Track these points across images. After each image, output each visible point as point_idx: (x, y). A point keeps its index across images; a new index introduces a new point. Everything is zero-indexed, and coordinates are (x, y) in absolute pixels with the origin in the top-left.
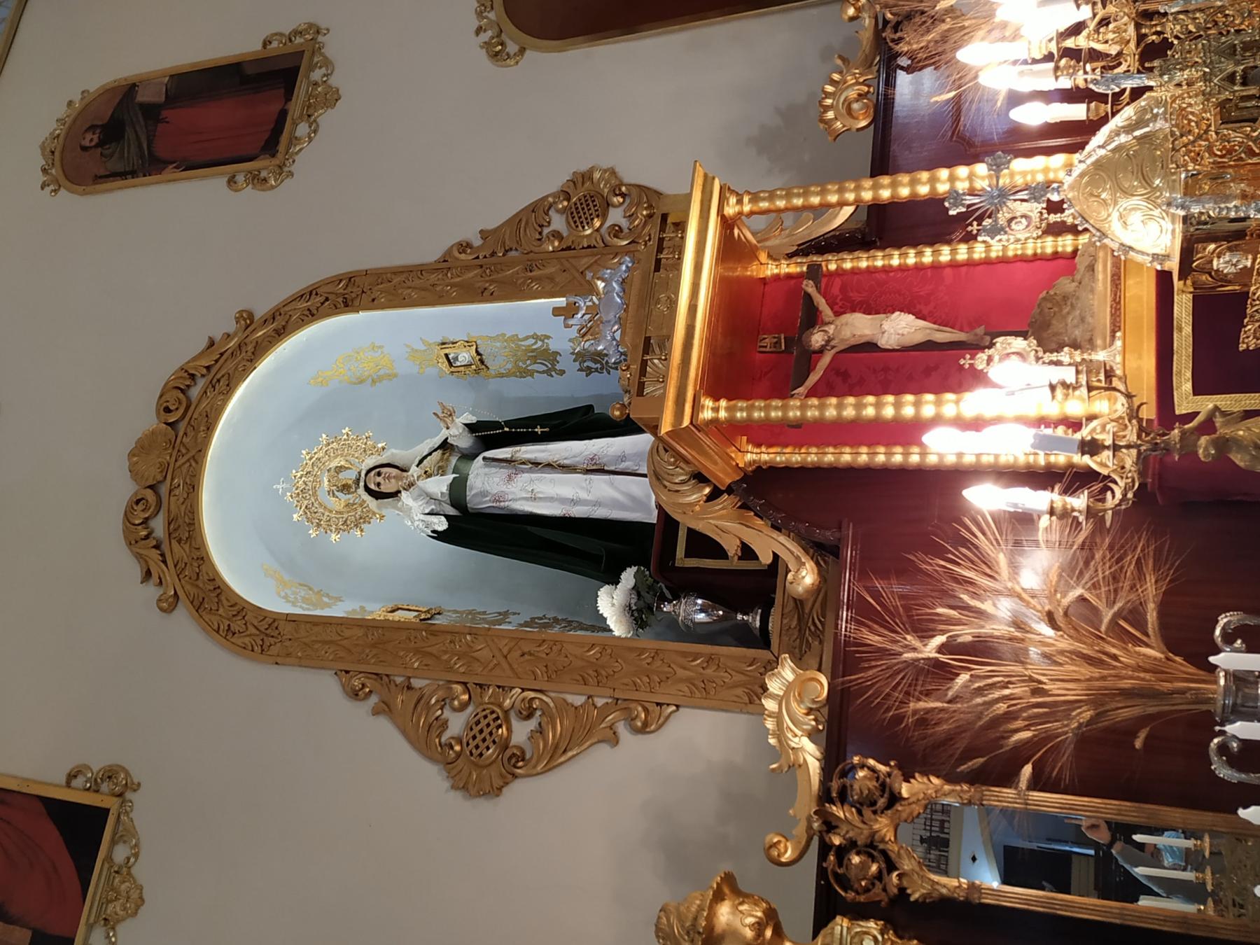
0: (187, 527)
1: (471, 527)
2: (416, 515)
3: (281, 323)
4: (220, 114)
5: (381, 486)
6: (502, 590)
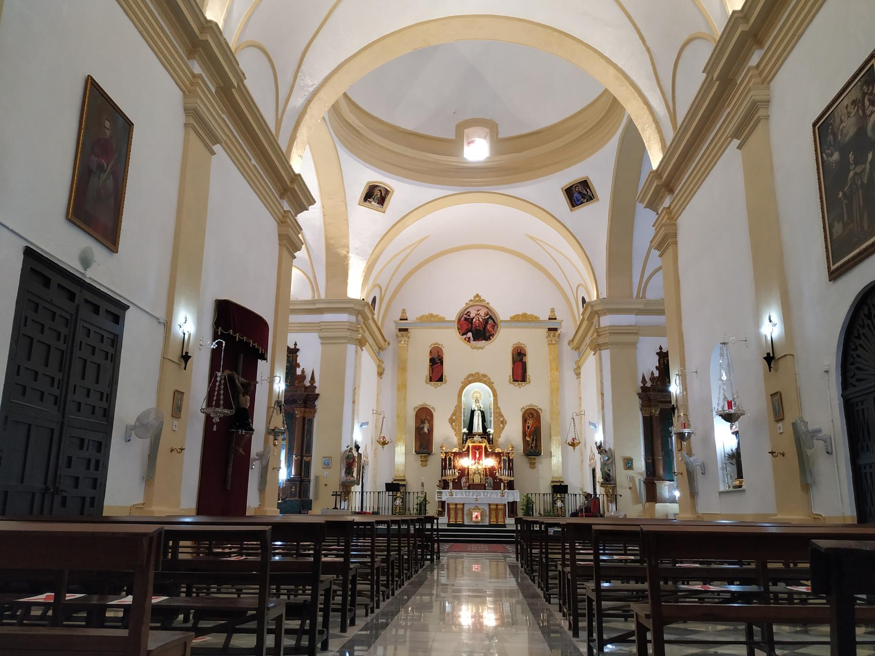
0: (470, 382)
1: (473, 412)
2: (474, 407)
3: (492, 388)
4: (520, 371)
5: (477, 401)
6: (464, 417)
